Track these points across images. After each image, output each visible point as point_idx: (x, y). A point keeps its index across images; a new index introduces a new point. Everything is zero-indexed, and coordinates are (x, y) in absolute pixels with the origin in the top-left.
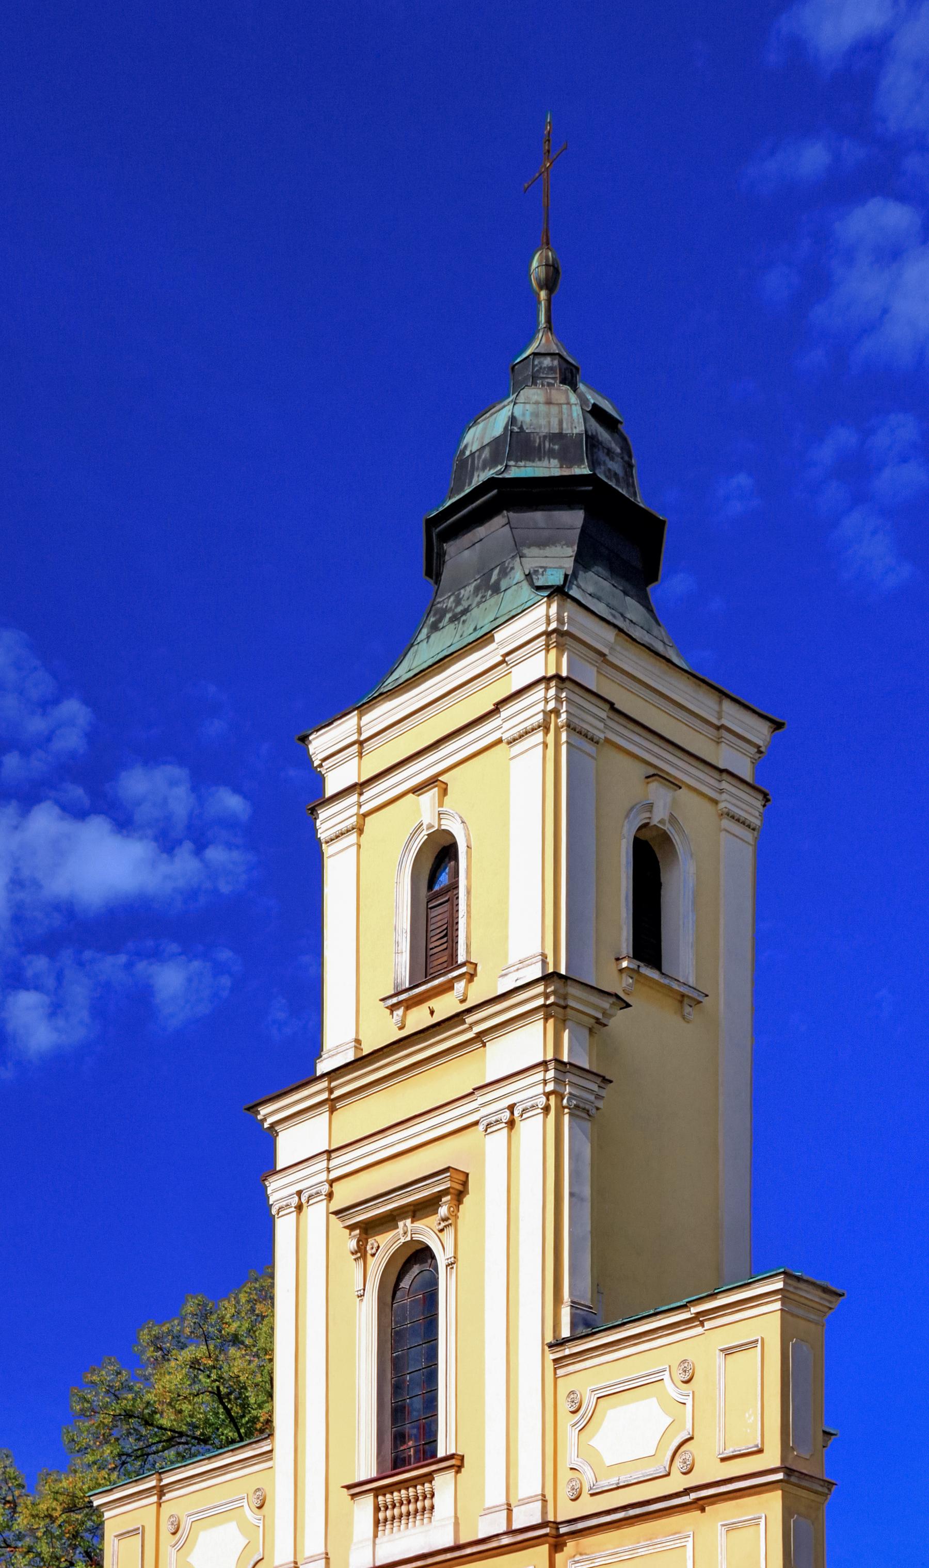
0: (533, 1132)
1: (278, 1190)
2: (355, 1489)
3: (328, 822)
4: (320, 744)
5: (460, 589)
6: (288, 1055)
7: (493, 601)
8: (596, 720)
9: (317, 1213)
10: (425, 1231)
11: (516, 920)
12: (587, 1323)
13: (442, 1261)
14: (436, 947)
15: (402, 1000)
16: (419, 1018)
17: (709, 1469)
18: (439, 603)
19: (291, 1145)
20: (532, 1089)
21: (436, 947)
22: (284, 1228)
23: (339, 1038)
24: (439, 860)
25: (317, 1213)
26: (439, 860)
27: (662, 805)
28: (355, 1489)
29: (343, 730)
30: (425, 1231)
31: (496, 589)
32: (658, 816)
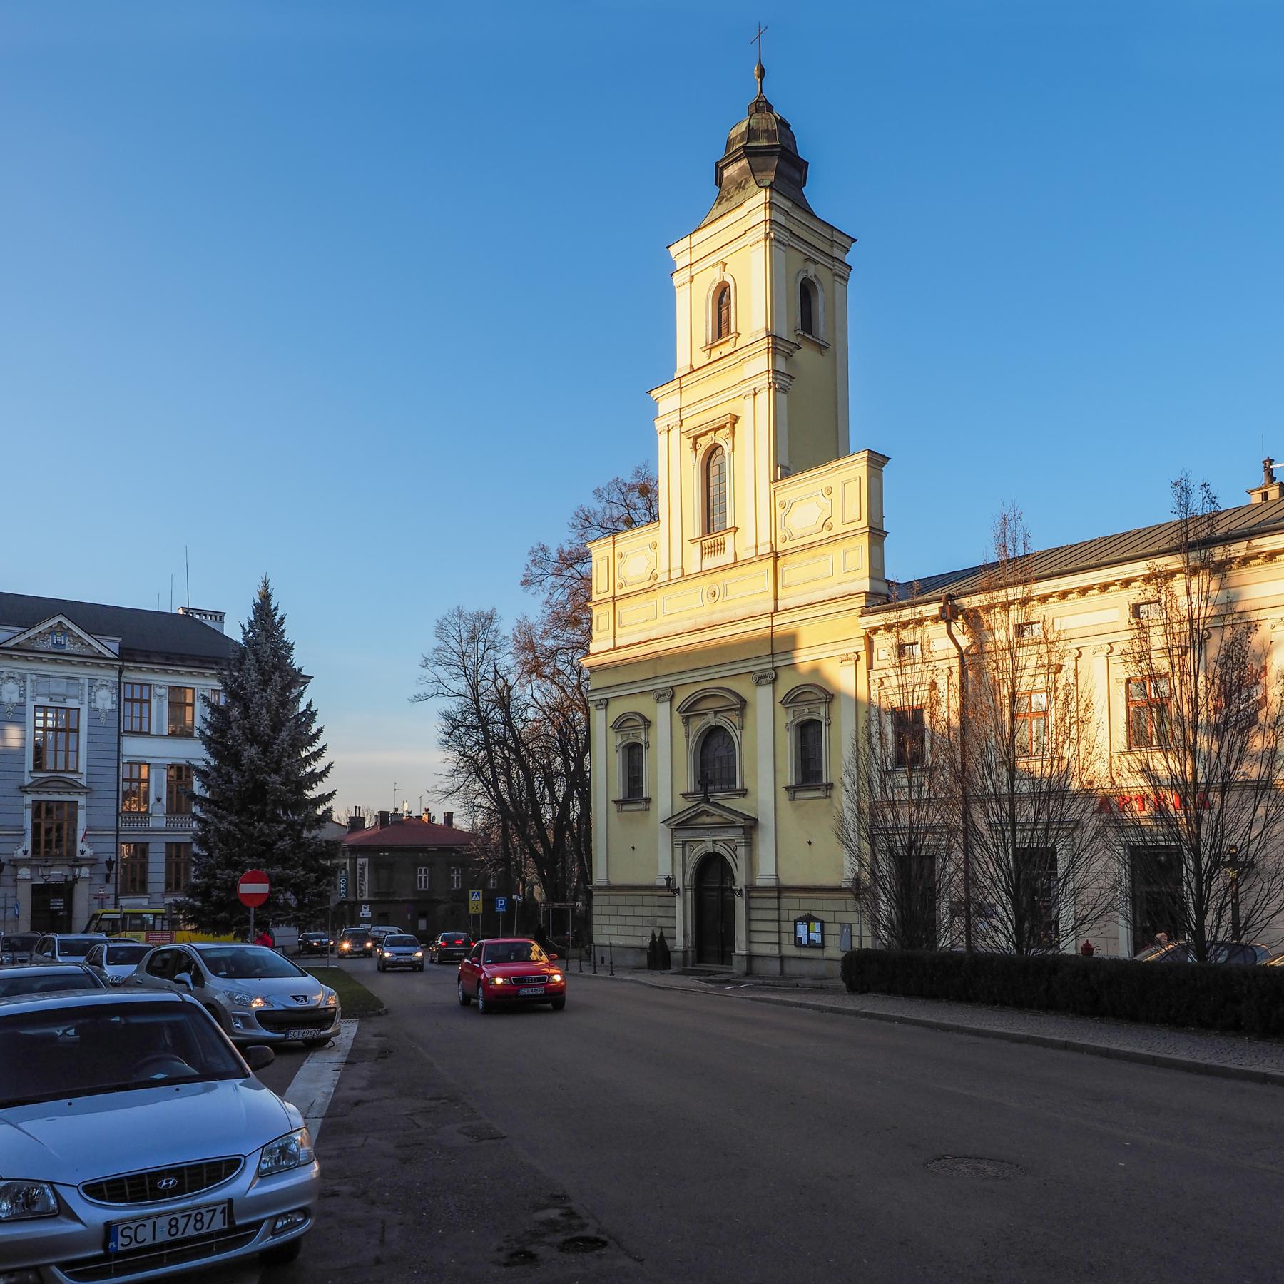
0: (764, 399)
1: (660, 425)
2: (693, 541)
3: (678, 279)
4: (674, 250)
5: (1012, 772)
6: (662, 369)
7: (742, 192)
8: (784, 236)
9: (675, 433)
10: (720, 438)
11: (754, 313)
12: (787, 473)
13: (727, 450)
14: (722, 326)
15: (710, 347)
16: (716, 354)
17: (839, 528)
18: (307, 760)
19: (663, 407)
20: (763, 382)
21: (722, 326)
22: (662, 439)
23: (682, 364)
24: (722, 295)
25: (675, 433)
26: (722, 295)
27: (812, 270)
28: (693, 541)
29: (685, 243)
30: (720, 438)
31: (744, 188)
32: (811, 273)
